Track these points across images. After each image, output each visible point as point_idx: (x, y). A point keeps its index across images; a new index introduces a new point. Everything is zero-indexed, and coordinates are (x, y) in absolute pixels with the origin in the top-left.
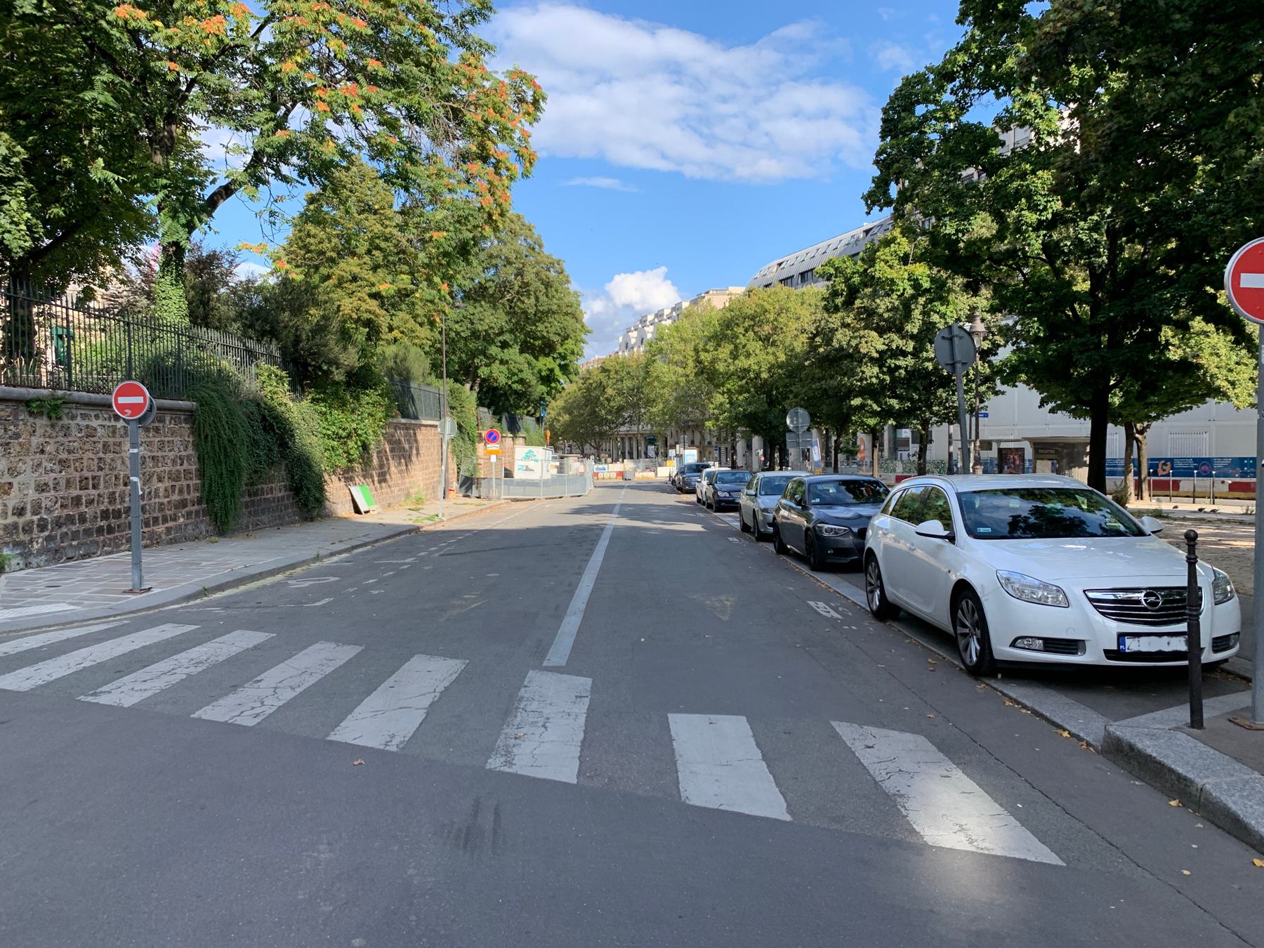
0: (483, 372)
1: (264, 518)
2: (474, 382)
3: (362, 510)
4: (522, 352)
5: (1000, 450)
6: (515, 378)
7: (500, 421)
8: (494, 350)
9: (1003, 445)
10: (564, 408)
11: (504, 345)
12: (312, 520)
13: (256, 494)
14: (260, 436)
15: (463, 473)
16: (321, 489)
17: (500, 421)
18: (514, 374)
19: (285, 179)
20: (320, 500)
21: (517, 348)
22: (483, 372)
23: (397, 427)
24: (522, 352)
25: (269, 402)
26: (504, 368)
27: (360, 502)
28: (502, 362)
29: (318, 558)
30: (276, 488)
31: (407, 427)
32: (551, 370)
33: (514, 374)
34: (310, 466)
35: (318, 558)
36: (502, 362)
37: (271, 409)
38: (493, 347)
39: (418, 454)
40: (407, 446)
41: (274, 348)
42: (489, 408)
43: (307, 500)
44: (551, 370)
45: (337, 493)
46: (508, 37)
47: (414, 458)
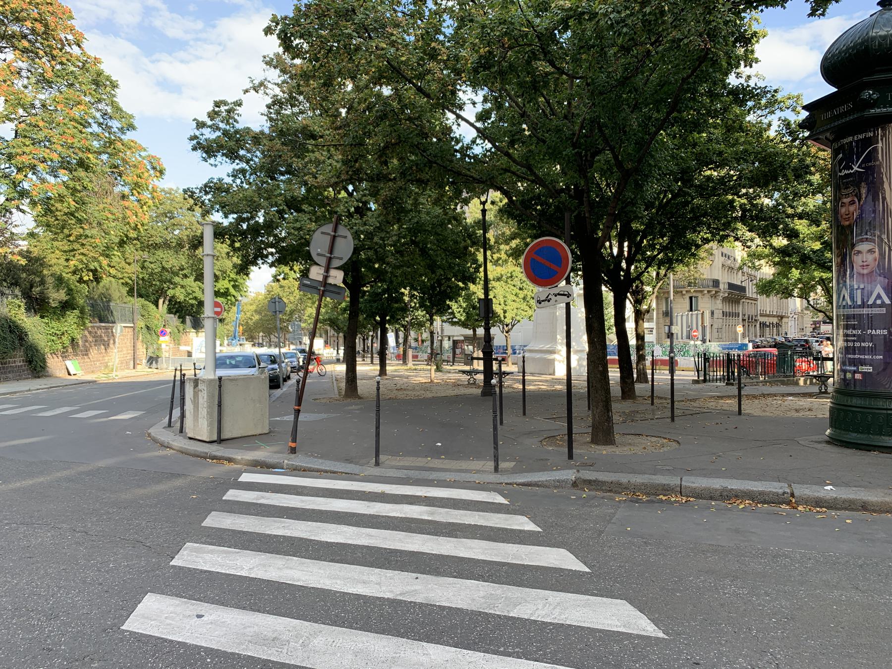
0: (170, 293)
1: (10, 375)
2: (165, 298)
3: (72, 373)
4: (195, 280)
5: (454, 341)
6: (191, 296)
7: (184, 322)
8: (177, 279)
9: (455, 338)
10: (256, 311)
11: (185, 276)
12: (39, 377)
13: (5, 364)
14: (8, 335)
15: (150, 354)
16: (44, 361)
17: (184, 322)
18: (189, 294)
19: (23, 212)
20: (44, 367)
21: (192, 278)
22: (170, 293)
23: (99, 328)
24: (195, 280)
25: (13, 319)
26: (183, 290)
27: (69, 368)
28: (182, 287)
29: (29, 390)
30: (18, 360)
31: (106, 328)
32: (227, 289)
33: (189, 294)
34: (37, 350)
35: (29, 390)
36: (182, 287)
37: (14, 322)
38: (177, 278)
39: (114, 343)
40: (106, 339)
41: (17, 291)
42: (175, 314)
43: (35, 365)
44: (227, 289)
45: (54, 364)
46: (230, 40)
47: (111, 346)
